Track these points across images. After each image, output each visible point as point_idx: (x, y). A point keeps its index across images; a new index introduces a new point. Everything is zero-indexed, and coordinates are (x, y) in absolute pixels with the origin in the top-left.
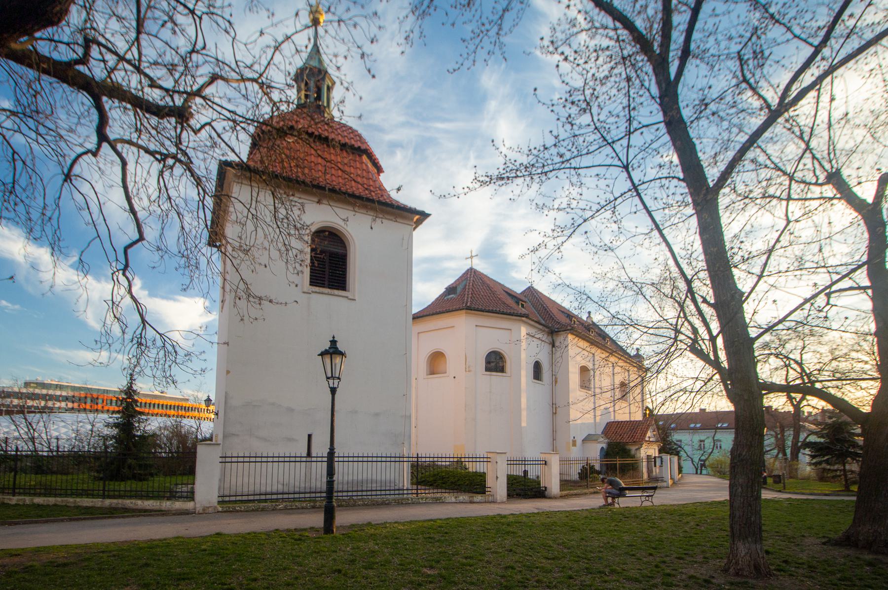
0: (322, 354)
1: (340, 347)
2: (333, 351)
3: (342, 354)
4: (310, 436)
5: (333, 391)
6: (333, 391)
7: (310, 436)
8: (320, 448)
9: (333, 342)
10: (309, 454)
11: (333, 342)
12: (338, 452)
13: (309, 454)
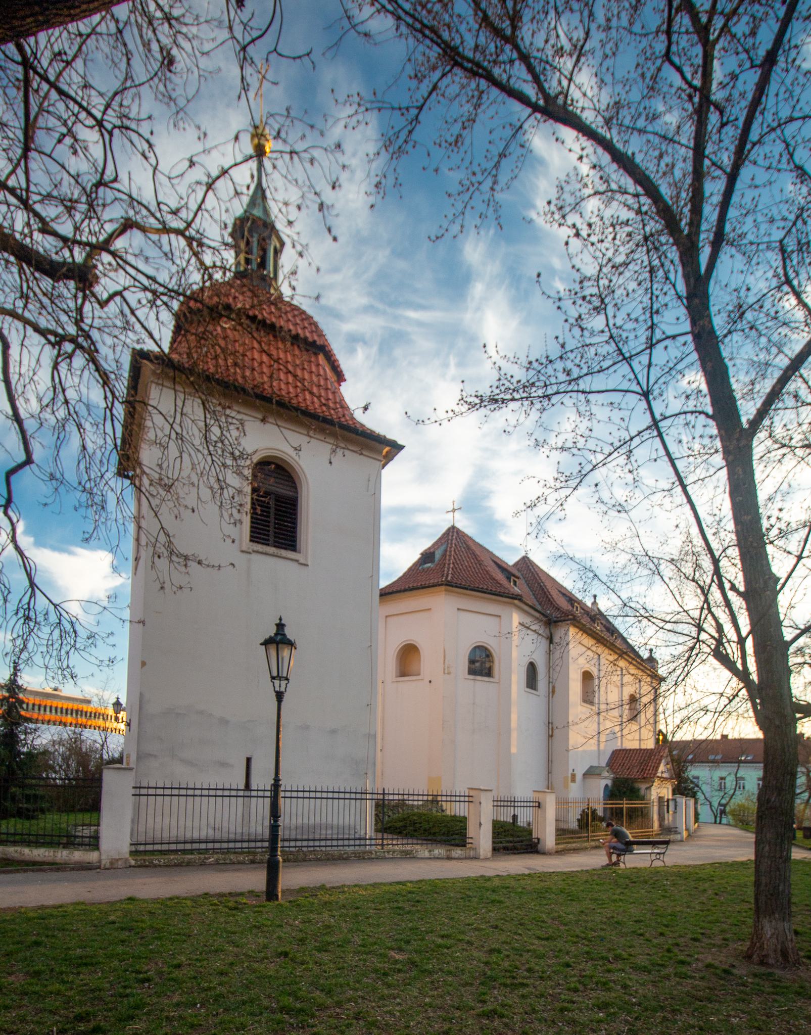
0: (267, 643)
1: (289, 633)
2: (279, 640)
3: (291, 644)
4: (249, 760)
5: (280, 696)
6: (280, 696)
7: (249, 760)
8: (262, 780)
9: (280, 626)
10: (248, 786)
11: (280, 626)
12: (285, 783)
13: (248, 786)
